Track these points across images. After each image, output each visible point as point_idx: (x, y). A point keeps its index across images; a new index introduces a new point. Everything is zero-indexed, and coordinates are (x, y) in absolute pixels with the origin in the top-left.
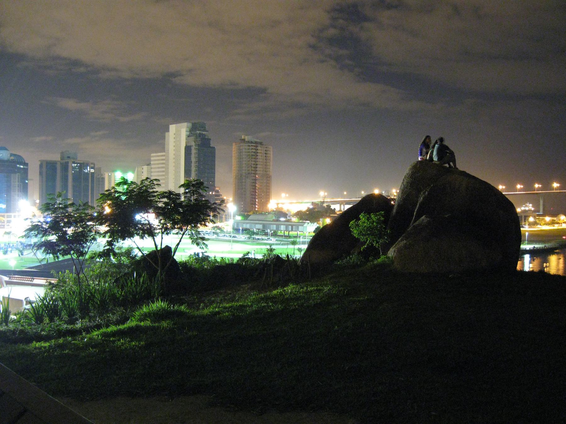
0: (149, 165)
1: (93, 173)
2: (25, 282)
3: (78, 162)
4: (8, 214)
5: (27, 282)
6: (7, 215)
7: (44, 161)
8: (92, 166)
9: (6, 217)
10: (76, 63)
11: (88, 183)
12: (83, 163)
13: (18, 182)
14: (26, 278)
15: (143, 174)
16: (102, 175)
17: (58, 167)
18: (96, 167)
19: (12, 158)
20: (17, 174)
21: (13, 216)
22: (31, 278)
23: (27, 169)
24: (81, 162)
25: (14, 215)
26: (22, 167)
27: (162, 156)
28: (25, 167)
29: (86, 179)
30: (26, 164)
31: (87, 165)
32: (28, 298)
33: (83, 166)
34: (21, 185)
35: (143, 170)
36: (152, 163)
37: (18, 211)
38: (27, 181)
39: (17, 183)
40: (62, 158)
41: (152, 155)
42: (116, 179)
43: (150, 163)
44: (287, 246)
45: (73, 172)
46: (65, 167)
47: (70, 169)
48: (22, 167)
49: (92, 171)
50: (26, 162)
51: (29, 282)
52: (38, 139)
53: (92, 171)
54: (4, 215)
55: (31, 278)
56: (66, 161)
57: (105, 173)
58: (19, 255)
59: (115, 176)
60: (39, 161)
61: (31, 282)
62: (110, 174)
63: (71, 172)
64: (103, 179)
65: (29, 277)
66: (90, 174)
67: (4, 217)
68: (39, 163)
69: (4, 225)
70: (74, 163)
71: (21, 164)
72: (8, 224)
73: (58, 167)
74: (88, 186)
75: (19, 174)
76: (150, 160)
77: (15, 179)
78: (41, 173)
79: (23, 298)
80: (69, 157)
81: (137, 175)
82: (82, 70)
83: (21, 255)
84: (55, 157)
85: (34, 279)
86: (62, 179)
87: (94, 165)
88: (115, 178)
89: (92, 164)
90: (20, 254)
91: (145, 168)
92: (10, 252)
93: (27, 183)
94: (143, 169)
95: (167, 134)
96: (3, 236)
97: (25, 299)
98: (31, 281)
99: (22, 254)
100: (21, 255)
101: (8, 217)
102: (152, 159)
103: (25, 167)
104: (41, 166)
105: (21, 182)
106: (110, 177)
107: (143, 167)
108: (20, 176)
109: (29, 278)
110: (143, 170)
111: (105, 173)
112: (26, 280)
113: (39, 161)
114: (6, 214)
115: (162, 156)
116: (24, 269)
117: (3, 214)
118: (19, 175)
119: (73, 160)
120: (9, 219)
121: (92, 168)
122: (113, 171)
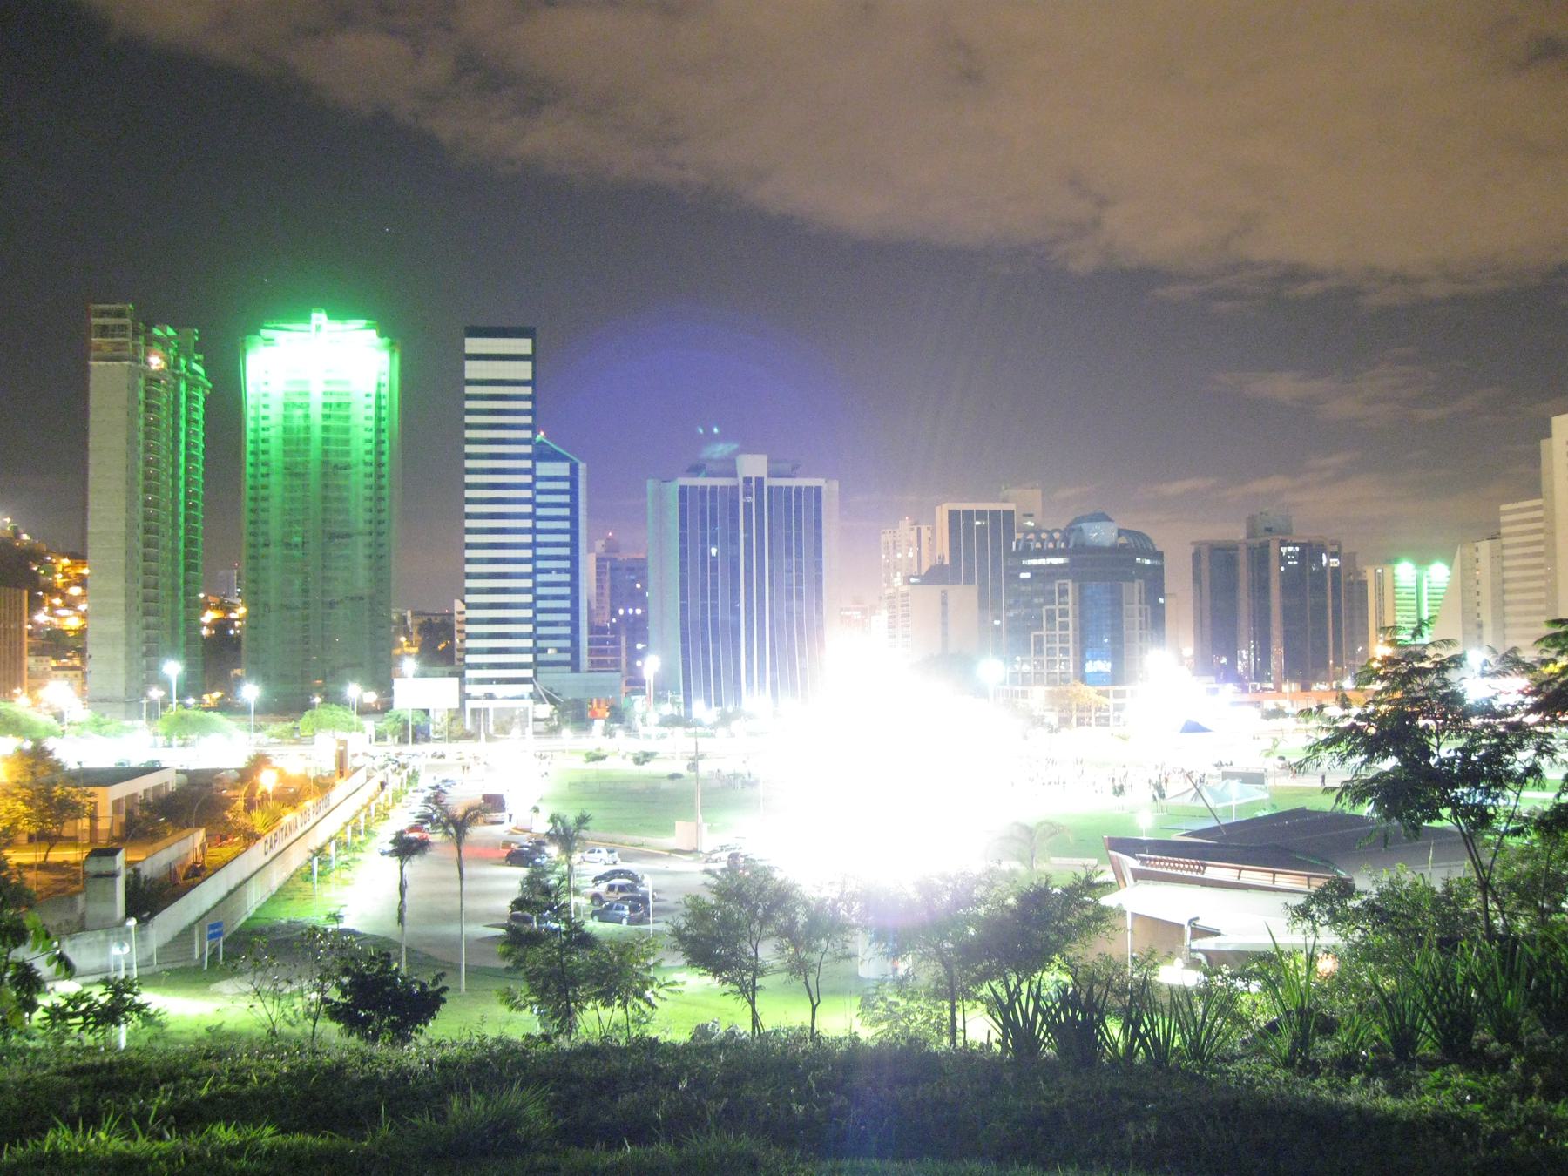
0: (1494, 537)
1: (1336, 570)
2: (1184, 873)
3: (1296, 541)
4: (1117, 688)
5: (1189, 874)
6: (1114, 691)
7: (1204, 543)
8: (1335, 549)
9: (1111, 695)
10: (1294, 274)
11: (1325, 595)
12: (1309, 544)
13: (1140, 602)
14: (1180, 862)
15: (1477, 566)
16: (1359, 574)
17: (1242, 557)
18: (1345, 550)
19: (1123, 540)
20: (1137, 582)
21: (1128, 693)
22: (1197, 864)
23: (1161, 568)
24: (1303, 541)
25: (1114, 691)
26: (1148, 562)
27: (1536, 508)
28: (1157, 562)
29: (1319, 587)
30: (1159, 555)
31: (1321, 548)
32: (1197, 919)
33: (1310, 552)
34: (1146, 609)
35: (1477, 555)
36: (1504, 530)
37: (1141, 680)
38: (1161, 600)
39: (1136, 606)
40: (1251, 534)
41: (1504, 507)
42: (1397, 584)
43: (1499, 534)
44: (1278, 784)
45: (1282, 569)
46: (1260, 557)
47: (1274, 562)
48: (1148, 562)
49: (1335, 563)
50: (1158, 549)
51: (1194, 874)
52: (1175, 488)
53: (1335, 563)
54: (1108, 691)
55: (1197, 864)
56: (1262, 540)
57: (1365, 568)
58: (1154, 798)
59: (1394, 575)
60: (1192, 543)
61: (1199, 875)
62: (1379, 571)
63: (1276, 570)
64: (1363, 584)
65: (1193, 861)
66: (1329, 572)
67: (1108, 697)
68: (1191, 550)
69: (1107, 719)
70: (1284, 543)
71: (1145, 556)
72: (1117, 714)
73: (1242, 557)
74: (1325, 607)
75: (1142, 581)
76: (1498, 524)
77: (1133, 591)
78: (1197, 578)
79: (1183, 920)
80: (1269, 530)
81: (1463, 569)
82: (1312, 288)
83: (1158, 798)
84: (1236, 532)
85: (1205, 866)
86: (1253, 591)
87: (1340, 548)
88: (1394, 581)
89: (1333, 544)
90: (1156, 794)
91: (1485, 546)
92: (351, 763)
93: (1163, 605)
94: (1477, 550)
95: (1544, 443)
96: (733, 735)
97: (1190, 922)
98: (1199, 871)
99: (1162, 796)
100: (1158, 798)
101: (1117, 695)
102: (1503, 519)
103: (1157, 562)
104: (1196, 557)
105: (1146, 603)
106: (1379, 579)
107: (1478, 544)
108: (1143, 587)
109: (1193, 864)
110: (1477, 555)
111: (1365, 568)
112: (1186, 868)
113: (1192, 543)
114: (1111, 689)
115: (1536, 508)
116: (1175, 837)
117: (1104, 688)
118: (1140, 584)
119: (1280, 537)
120: (1119, 701)
121: (1334, 555)
122: (1391, 561)
